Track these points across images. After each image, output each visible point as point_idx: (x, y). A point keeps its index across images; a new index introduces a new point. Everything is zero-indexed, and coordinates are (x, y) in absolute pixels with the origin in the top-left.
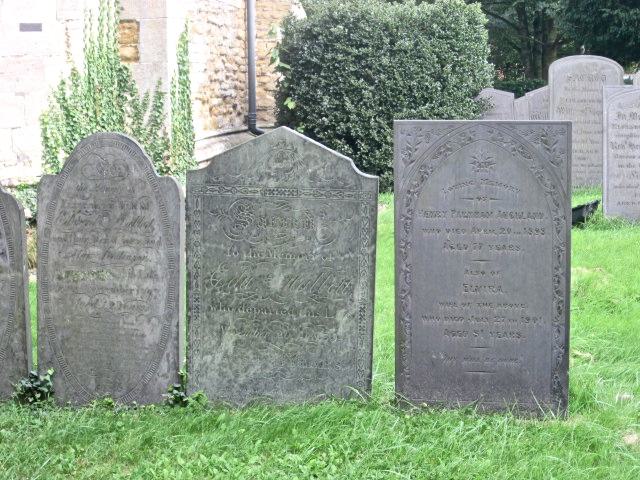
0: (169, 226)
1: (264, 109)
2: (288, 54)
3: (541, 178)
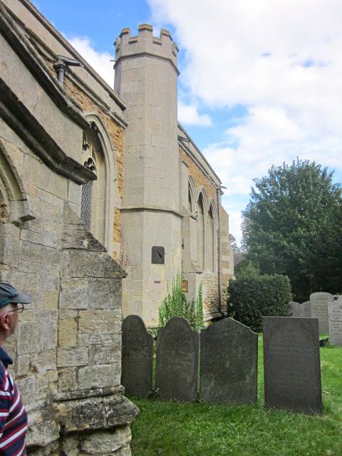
0: (196, 346)
1: (224, 306)
2: (230, 290)
3: (309, 336)
